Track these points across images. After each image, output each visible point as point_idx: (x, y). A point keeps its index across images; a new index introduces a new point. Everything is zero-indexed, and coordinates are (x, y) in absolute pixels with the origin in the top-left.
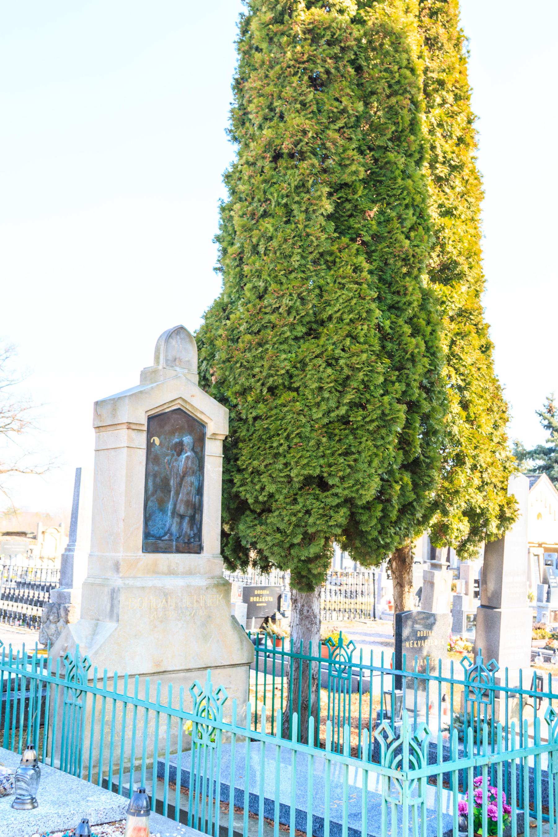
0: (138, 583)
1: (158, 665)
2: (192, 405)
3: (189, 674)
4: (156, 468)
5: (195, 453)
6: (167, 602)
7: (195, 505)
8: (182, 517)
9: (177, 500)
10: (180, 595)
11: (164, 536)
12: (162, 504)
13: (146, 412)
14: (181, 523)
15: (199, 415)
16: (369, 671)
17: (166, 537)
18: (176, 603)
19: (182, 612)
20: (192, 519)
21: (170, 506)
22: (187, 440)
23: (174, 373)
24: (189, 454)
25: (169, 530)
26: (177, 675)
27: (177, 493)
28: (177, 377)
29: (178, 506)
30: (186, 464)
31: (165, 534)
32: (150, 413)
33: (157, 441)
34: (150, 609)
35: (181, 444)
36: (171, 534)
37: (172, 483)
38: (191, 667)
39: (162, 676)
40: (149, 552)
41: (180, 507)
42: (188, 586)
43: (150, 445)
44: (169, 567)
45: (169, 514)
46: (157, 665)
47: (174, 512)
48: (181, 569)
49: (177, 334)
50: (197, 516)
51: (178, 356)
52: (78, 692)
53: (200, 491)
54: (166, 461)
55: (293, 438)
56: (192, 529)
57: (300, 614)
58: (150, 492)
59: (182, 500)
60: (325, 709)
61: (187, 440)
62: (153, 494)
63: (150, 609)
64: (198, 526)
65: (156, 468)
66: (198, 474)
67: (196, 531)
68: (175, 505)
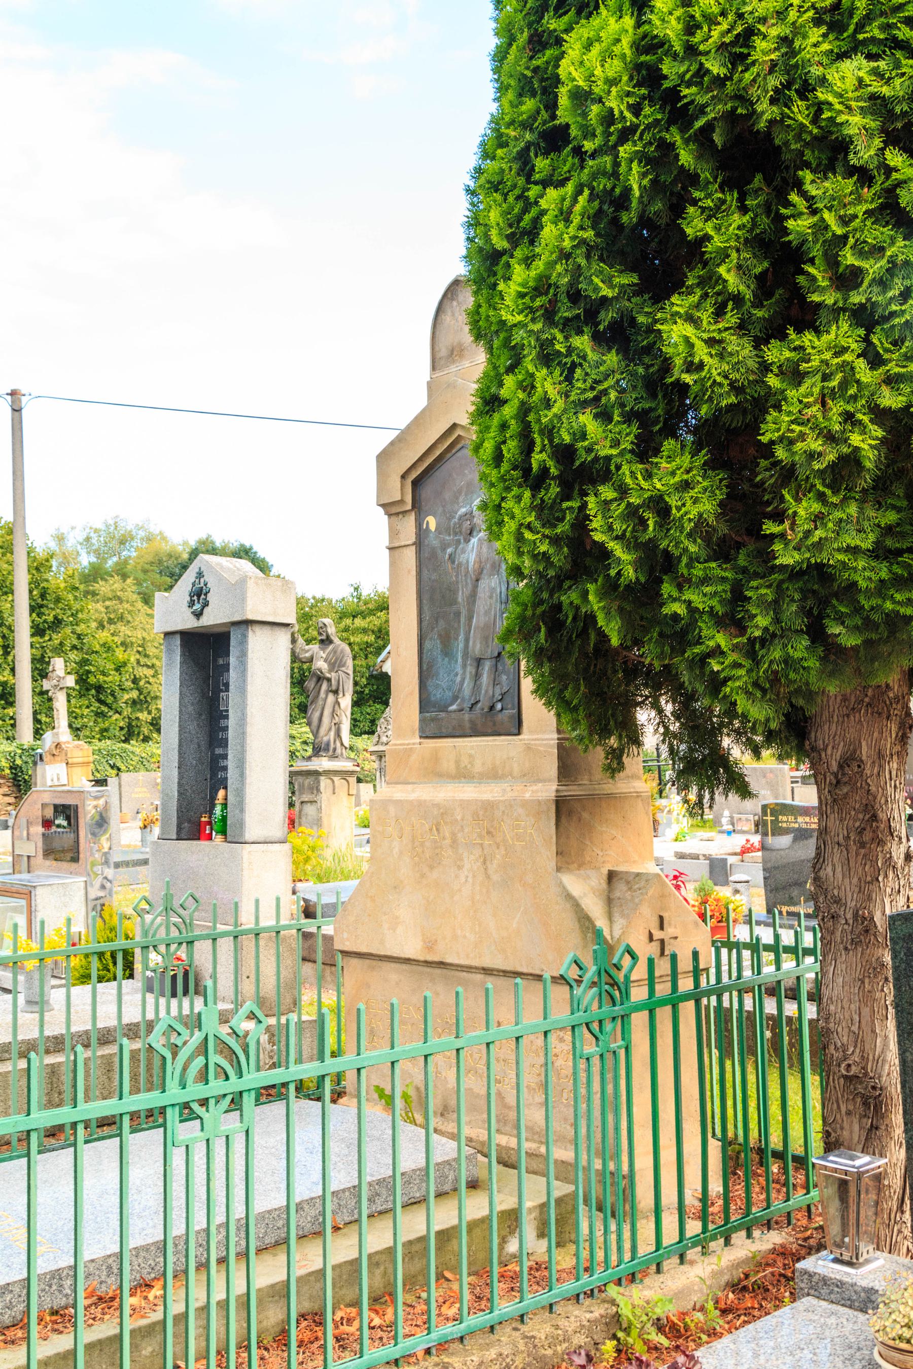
1: (430, 946)
11: (452, 704)
12: (447, 641)
13: (403, 477)
14: (477, 676)
16: (209, 942)
24: (482, 534)
30: (479, 554)
32: (414, 475)
36: (463, 700)
38: (449, 960)
44: (457, 762)
47: (466, 654)
48: (478, 768)
52: (595, 1027)
59: (477, 627)
60: (311, 1004)
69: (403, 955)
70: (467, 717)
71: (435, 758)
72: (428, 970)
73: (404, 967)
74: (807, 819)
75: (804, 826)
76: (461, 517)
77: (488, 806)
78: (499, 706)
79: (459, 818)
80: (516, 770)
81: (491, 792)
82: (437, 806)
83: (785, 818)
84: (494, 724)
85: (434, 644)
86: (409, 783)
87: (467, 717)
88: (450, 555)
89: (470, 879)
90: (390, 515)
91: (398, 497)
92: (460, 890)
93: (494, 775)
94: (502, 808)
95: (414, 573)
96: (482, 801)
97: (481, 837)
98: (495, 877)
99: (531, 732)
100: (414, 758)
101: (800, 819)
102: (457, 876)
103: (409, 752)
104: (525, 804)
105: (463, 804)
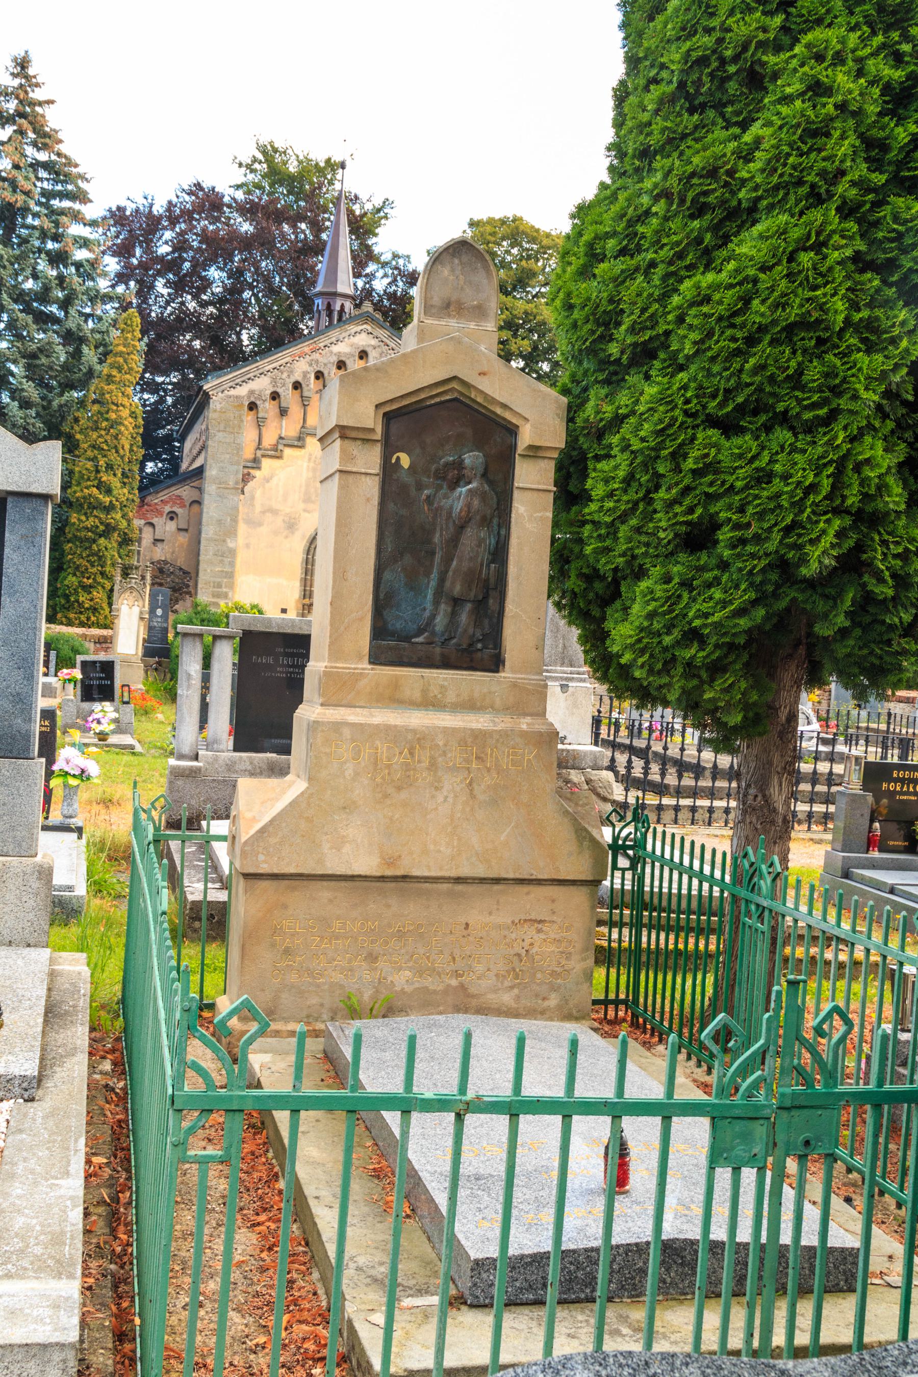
2: (482, 392)
3: (460, 887)
5: (491, 483)
6: (411, 754)
7: (487, 580)
8: (456, 602)
9: (447, 571)
11: (417, 636)
13: (377, 406)
14: (454, 614)
15: (499, 411)
20: (481, 605)
22: (472, 458)
26: (435, 885)
29: (448, 584)
30: (469, 506)
31: (419, 632)
32: (388, 408)
33: (405, 460)
34: (376, 764)
35: (459, 465)
36: (433, 633)
37: (436, 539)
40: (381, 664)
41: (453, 583)
43: (389, 470)
46: (390, 865)
47: (439, 593)
48: (451, 697)
49: (453, 256)
50: (491, 601)
53: (500, 554)
54: (424, 497)
56: (477, 623)
57: (744, 804)
61: (472, 458)
63: (376, 764)
65: (404, 512)
66: (495, 521)
67: (487, 630)
68: (442, 580)
69: (350, 873)
70: (438, 650)
71: (395, 685)
72: (378, 884)
73: (343, 884)
76: (447, 464)
77: (479, 736)
79: (441, 743)
80: (498, 703)
81: (479, 722)
82: (414, 731)
84: (471, 661)
85: (394, 577)
86: (355, 707)
87: (438, 650)
88: (428, 497)
89: (450, 800)
91: (370, 424)
92: (436, 809)
93: (471, 706)
94: (496, 736)
96: (472, 730)
97: (468, 761)
98: (481, 797)
99: (513, 672)
100: (362, 683)
102: (433, 797)
103: (357, 677)
104: (523, 734)
105: (445, 730)
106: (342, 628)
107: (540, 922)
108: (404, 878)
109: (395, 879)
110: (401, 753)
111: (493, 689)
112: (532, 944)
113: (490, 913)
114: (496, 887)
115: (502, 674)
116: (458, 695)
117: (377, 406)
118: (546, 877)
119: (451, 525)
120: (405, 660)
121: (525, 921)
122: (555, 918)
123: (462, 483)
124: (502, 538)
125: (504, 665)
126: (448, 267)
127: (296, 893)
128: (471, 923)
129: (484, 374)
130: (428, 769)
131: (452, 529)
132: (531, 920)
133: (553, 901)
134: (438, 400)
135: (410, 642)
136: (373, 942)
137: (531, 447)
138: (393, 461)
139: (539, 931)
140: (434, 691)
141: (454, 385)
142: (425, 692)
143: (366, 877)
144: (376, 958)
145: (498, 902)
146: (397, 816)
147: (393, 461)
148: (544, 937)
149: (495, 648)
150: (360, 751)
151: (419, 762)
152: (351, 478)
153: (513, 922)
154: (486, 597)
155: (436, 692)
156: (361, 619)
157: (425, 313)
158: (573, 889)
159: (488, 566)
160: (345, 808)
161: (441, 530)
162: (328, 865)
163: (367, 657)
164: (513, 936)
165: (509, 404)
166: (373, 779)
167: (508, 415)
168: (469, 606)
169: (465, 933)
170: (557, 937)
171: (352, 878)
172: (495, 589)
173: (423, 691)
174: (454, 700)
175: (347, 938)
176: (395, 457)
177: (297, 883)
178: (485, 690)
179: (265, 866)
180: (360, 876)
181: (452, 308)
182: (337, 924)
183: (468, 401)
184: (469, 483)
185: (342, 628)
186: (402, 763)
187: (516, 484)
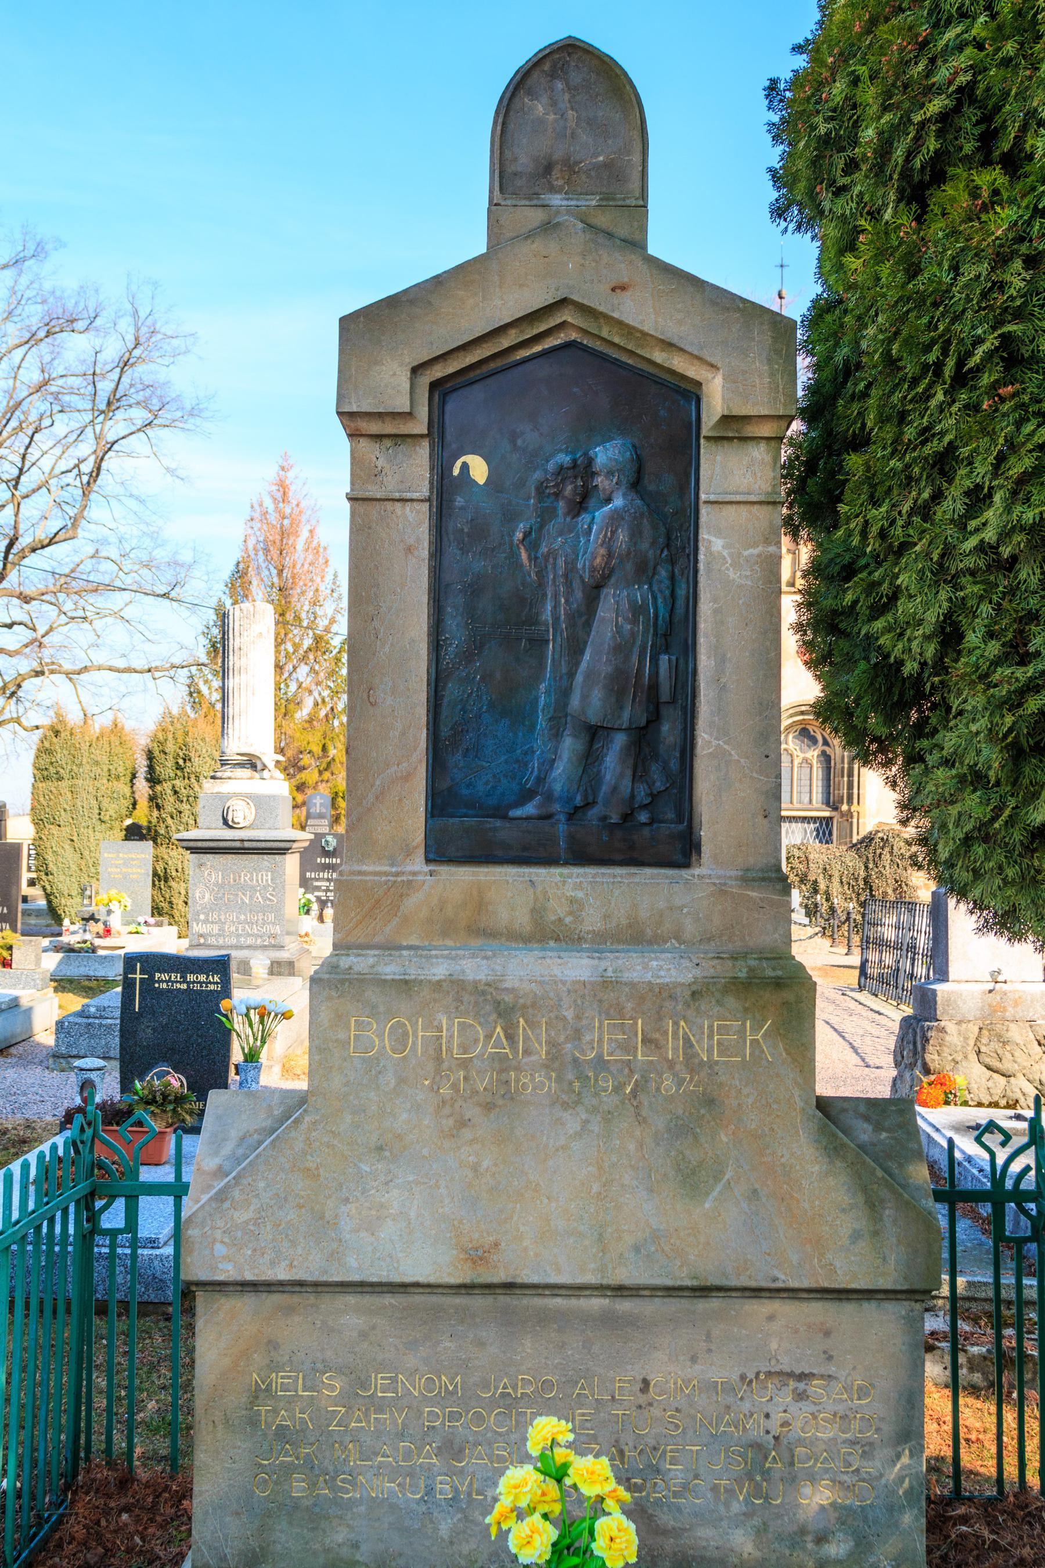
0: (390, 970)
1: (477, 1256)
2: (620, 323)
3: (625, 1306)
4: (480, 565)
7: (654, 686)
9: (571, 675)
10: (569, 1014)
11: (521, 802)
13: (415, 370)
15: (659, 356)
17: (530, 809)
18: (552, 1044)
19: (583, 1078)
21: (543, 695)
23: (536, 217)
25: (541, 780)
26: (574, 1302)
27: (575, 649)
28: (548, 228)
29: (575, 701)
30: (608, 543)
31: (525, 796)
32: (438, 372)
33: (479, 469)
34: (439, 1059)
36: (549, 797)
39: (503, 1300)
40: (451, 861)
42: (606, 984)
45: (542, 721)
48: (592, 921)
49: (553, 75)
50: (665, 728)
51: (557, 156)
54: (519, 535)
55: (978, 369)
56: (639, 773)
58: (451, 651)
62: (468, 656)
63: (439, 1059)
64: (674, 765)
66: (663, 573)
69: (397, 1279)
72: (458, 1300)
73: (388, 1300)
74: (202, 978)
75: (197, 987)
78: (643, 817)
80: (690, 929)
83: (164, 977)
90: (353, 435)
91: (402, 404)
95: (424, 551)
100: (412, 901)
101: (190, 977)
106: (371, 798)
107: (802, 1377)
108: (509, 1287)
109: (489, 1288)
110: (488, 1037)
111: (678, 902)
112: (785, 1424)
113: (694, 1359)
114: (702, 1305)
115: (697, 871)
116: (606, 917)
117: (415, 370)
118: (806, 1284)
119: (576, 584)
120: (499, 853)
121: (769, 1374)
122: (832, 1370)
123: (592, 502)
124: (680, 610)
125: (699, 853)
126: (545, 99)
127: (297, 1319)
128: (654, 1379)
129: (623, 288)
130: (546, 1067)
131: (579, 594)
132: (780, 1373)
133: (827, 1334)
134: (537, 348)
135: (505, 817)
136: (453, 1418)
137: (727, 419)
138: (456, 472)
139: (801, 1396)
140: (557, 909)
141: (566, 315)
142: (537, 912)
143: (429, 1286)
144: (461, 1450)
145: (708, 1336)
146: (486, 1164)
147: (456, 472)
148: (813, 1408)
149: (680, 820)
150: (406, 1034)
151: (527, 1052)
152: (374, 510)
153: (743, 1377)
154: (655, 718)
155: (561, 912)
156: (407, 777)
157: (502, 190)
158: (869, 1308)
159: (655, 661)
160: (380, 1149)
161: (556, 596)
162: (352, 1261)
163: (421, 851)
164: (746, 1406)
165: (675, 341)
166: (434, 1089)
167: (678, 364)
168: (620, 740)
169: (642, 1399)
170: (841, 1409)
171: (404, 1288)
172: (673, 702)
173: (533, 910)
174: (599, 926)
175: (400, 1411)
176: (458, 464)
177: (296, 1299)
178: (662, 905)
179: (229, 1267)
180: (417, 1285)
181: (556, 173)
182: (380, 1380)
183: (598, 345)
184: (609, 500)
185: (371, 798)
186: (493, 1057)
187: (703, 497)
